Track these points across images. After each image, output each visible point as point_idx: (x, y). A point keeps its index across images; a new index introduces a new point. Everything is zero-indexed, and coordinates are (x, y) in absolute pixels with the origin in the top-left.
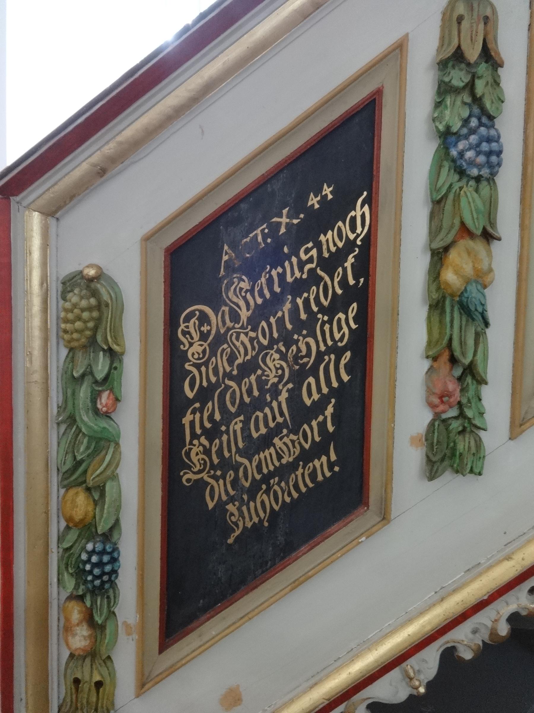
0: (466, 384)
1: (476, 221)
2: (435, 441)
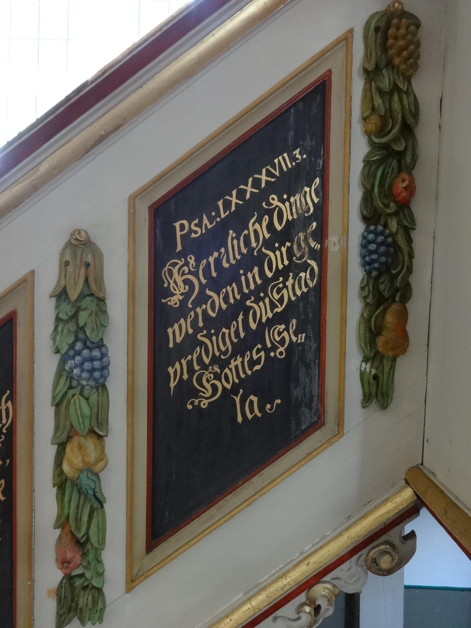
0: (86, 550)
1: (81, 424)
2: (63, 596)
